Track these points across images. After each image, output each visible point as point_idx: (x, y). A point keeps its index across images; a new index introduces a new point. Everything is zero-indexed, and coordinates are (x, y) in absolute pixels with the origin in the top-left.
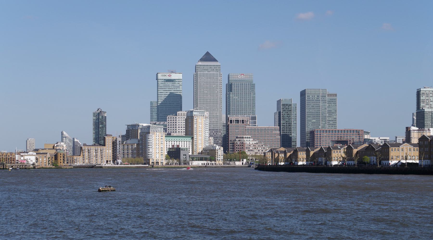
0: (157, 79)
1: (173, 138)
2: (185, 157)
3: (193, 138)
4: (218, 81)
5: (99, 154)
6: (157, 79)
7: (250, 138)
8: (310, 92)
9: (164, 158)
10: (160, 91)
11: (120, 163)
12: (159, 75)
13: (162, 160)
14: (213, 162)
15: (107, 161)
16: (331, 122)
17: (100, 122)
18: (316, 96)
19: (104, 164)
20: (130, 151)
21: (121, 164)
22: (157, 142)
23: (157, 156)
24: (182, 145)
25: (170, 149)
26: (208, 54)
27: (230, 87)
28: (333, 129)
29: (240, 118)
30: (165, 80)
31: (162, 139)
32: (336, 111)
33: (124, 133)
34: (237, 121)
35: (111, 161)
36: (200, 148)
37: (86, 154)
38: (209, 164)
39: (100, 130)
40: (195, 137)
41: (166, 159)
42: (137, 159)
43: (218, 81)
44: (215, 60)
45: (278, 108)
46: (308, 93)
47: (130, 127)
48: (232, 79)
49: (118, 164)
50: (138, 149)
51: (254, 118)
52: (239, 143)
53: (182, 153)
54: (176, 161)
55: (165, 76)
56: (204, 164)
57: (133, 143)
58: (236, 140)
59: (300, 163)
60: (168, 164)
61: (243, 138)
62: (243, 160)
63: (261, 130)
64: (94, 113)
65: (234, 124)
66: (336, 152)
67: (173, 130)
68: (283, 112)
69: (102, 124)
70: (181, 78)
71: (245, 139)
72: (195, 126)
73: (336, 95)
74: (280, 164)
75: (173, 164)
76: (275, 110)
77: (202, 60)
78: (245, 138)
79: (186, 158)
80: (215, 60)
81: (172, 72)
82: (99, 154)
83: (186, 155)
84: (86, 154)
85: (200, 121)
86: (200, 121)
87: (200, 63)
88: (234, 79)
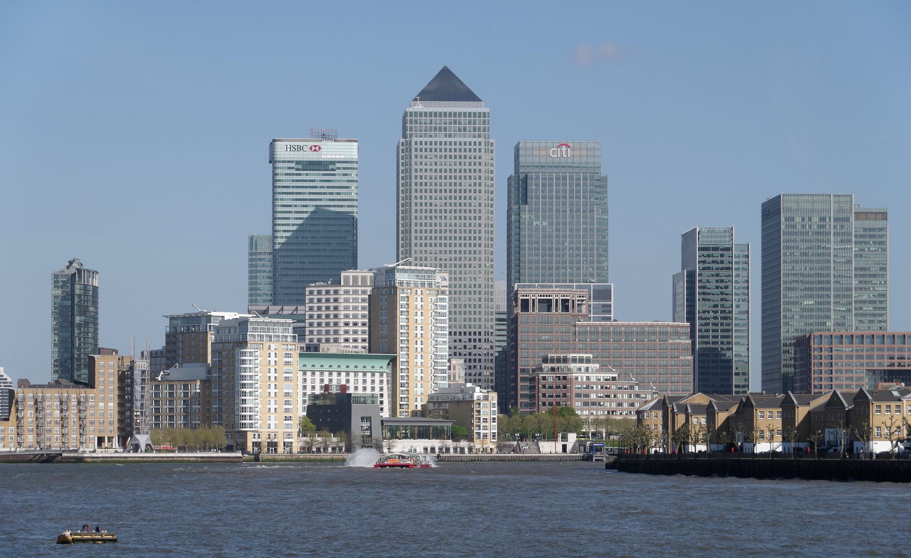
0: (272, 161)
1: (326, 363)
2: (366, 425)
3: (393, 361)
4: (483, 167)
5: (73, 414)
6: (272, 161)
7: (588, 361)
8: (794, 206)
9: (295, 430)
10: (284, 199)
11: (143, 447)
12: (280, 147)
13: (289, 435)
14: (464, 444)
15: (101, 440)
16: (869, 308)
17: (75, 307)
18: (816, 219)
19: (89, 450)
20: (180, 406)
21: (149, 448)
22: (273, 375)
23: (273, 422)
24: (357, 385)
25: (315, 397)
26: (445, 74)
27: (520, 188)
28: (875, 330)
29: (556, 293)
30: (298, 163)
31: (287, 363)
32: (884, 269)
33: (160, 344)
34: (547, 304)
35: (115, 440)
36: (418, 395)
37: (29, 414)
38: (448, 450)
39: (76, 331)
40: (401, 357)
41: (304, 432)
42: (204, 433)
43: (483, 167)
44: (469, 96)
45: (687, 258)
46: (789, 210)
47: (179, 322)
48: (529, 160)
49: (136, 448)
50: (205, 398)
51: (603, 294)
52: (550, 377)
53: (357, 412)
54: (335, 439)
55: (300, 148)
57: (189, 378)
58: (541, 369)
59: (762, 447)
60: (309, 450)
61: (565, 360)
62: (565, 438)
63: (628, 333)
64: (56, 276)
65: (535, 312)
66: (884, 408)
67: (327, 332)
68: (703, 271)
69: (84, 311)
70: (354, 156)
71: (572, 365)
72: (401, 320)
73: (884, 215)
74: (691, 449)
75: (325, 449)
76: (676, 267)
77: (426, 95)
78: (574, 360)
79: (370, 428)
80: (469, 96)
81: (324, 137)
82: (73, 414)
83: (369, 419)
84: (29, 414)
85: (419, 303)
86: (419, 303)
87: (420, 107)
88: (536, 160)
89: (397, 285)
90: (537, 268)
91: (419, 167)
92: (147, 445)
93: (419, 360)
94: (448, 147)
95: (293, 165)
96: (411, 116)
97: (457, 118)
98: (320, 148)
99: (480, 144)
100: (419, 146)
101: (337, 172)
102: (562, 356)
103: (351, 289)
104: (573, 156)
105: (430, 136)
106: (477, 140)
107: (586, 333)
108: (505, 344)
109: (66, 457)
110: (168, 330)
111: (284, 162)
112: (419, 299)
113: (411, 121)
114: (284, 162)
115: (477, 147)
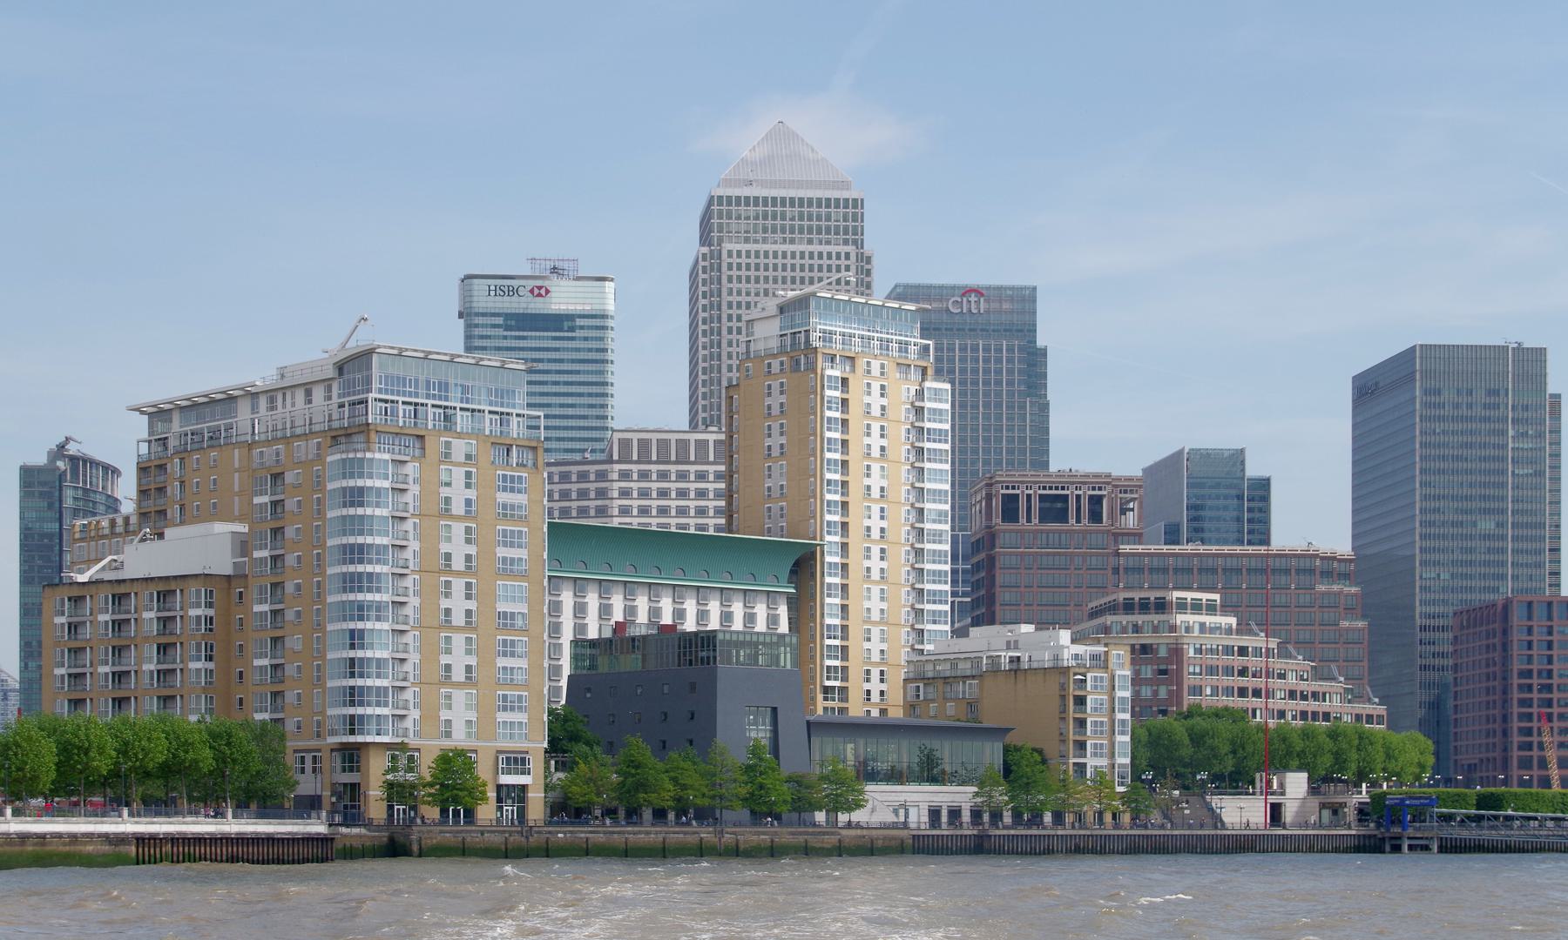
13: (517, 762)
30: (508, 316)
56: (955, 813)
65: (1031, 523)
71: (1180, 619)
89: (816, 343)
91: (735, 298)
93: (875, 564)
95: (500, 321)
96: (720, 204)
97: (805, 209)
98: (547, 292)
99: (847, 256)
101: (578, 333)
102: (1153, 595)
103: (635, 468)
104: (988, 311)
105: (756, 241)
106: (843, 249)
111: (484, 315)
112: (876, 387)
113: (720, 213)
114: (484, 315)
115: (843, 262)
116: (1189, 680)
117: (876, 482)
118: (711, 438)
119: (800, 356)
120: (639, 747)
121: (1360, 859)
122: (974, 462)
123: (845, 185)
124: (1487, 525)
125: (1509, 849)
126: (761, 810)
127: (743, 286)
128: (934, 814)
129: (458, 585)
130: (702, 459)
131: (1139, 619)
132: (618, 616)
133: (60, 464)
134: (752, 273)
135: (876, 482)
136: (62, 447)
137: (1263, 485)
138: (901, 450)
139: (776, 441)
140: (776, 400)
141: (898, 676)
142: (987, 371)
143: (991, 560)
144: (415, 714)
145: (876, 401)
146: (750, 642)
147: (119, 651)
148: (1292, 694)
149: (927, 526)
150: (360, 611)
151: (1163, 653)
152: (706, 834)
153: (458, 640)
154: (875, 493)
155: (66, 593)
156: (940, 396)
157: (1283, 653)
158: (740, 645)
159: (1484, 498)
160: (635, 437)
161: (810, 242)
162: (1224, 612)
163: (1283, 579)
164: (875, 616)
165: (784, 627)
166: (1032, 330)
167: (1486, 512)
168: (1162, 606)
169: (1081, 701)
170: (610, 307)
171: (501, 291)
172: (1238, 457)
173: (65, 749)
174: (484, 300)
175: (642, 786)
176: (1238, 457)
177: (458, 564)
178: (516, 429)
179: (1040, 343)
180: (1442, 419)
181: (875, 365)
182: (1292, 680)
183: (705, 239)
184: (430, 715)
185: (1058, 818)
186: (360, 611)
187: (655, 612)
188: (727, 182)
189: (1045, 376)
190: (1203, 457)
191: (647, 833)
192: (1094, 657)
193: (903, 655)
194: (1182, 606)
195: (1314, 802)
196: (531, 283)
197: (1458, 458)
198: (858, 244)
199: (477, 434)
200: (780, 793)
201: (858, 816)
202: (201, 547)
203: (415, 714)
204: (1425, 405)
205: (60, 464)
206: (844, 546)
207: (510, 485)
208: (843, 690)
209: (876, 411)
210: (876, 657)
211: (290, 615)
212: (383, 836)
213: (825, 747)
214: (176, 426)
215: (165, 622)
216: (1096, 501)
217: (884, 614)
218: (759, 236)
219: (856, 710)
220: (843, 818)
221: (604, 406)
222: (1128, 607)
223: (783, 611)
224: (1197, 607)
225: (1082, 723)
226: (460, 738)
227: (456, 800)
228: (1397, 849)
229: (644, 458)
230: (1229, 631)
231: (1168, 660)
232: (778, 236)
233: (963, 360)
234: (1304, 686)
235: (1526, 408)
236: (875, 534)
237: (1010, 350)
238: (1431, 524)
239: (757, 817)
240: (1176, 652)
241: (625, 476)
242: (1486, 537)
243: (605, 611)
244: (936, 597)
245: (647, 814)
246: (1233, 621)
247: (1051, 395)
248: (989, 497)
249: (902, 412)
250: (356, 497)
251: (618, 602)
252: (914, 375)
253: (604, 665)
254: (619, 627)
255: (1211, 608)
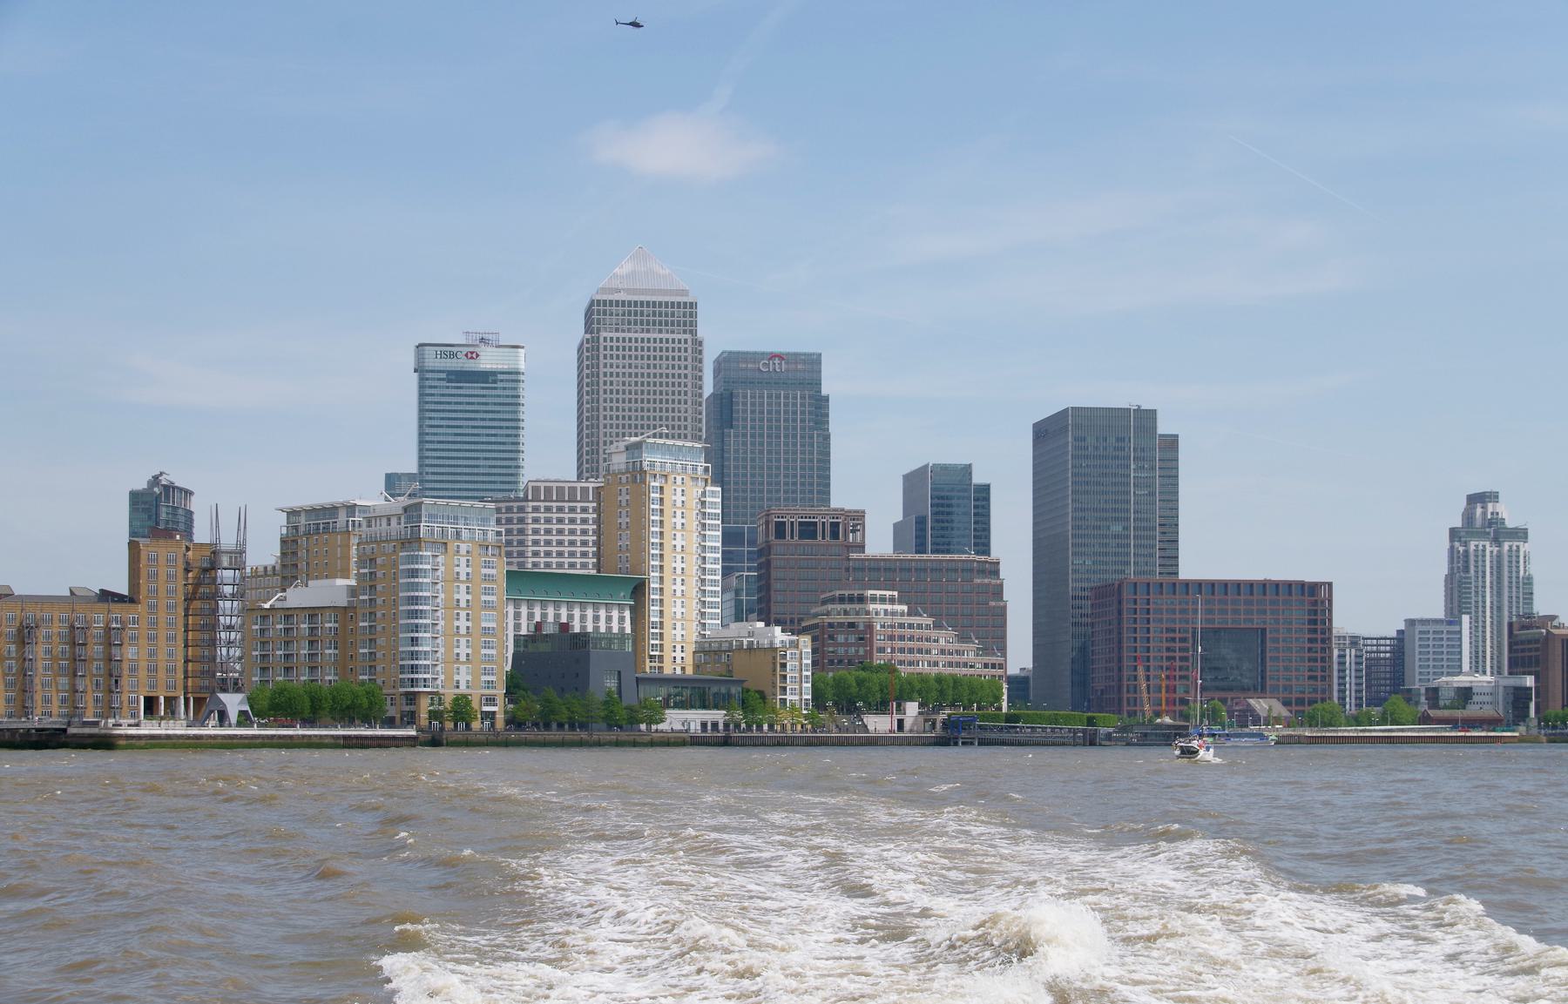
11: (233, 716)
13: (491, 700)
15: (151, 704)
18: (1112, 440)
21: (244, 719)
30: (449, 373)
47: (303, 520)
49: (223, 717)
56: (715, 725)
62: (900, 709)
71: (872, 607)
90: (761, 491)
91: (608, 370)
92: (242, 713)
93: (679, 588)
94: (646, 345)
95: (444, 376)
100: (609, 344)
101: (500, 385)
107: (863, 570)
108: (577, 630)
109: (74, 735)
110: (284, 531)
115: (683, 345)
116: (877, 644)
117: (679, 543)
118: (591, 486)
119: (637, 475)
120: (551, 693)
121: (937, 749)
122: (777, 476)
123: (684, 292)
124: (1117, 528)
125: (1003, 743)
126: (611, 723)
127: (614, 361)
128: (704, 725)
129: (463, 614)
130: (585, 499)
131: (848, 607)
132: (537, 618)
133: (156, 490)
134: (621, 353)
135: (679, 543)
136: (156, 478)
137: (984, 491)
138: (694, 525)
139: (624, 520)
140: (624, 498)
141: (691, 648)
142: (786, 412)
143: (768, 562)
144: (442, 677)
145: (679, 498)
146: (609, 638)
147: (287, 643)
148: (943, 652)
149: (708, 566)
150: (417, 628)
151: (861, 628)
152: (584, 735)
153: (463, 641)
154: (679, 549)
155: (259, 614)
156: (715, 495)
157: (937, 626)
158: (601, 639)
159: (1115, 510)
160: (542, 485)
161: (660, 331)
162: (900, 603)
163: (953, 575)
164: (679, 616)
165: (628, 630)
166: (818, 384)
167: (1116, 519)
168: (861, 599)
169: (784, 666)
170: (522, 366)
171: (444, 355)
172: (967, 470)
173: (312, 699)
174: (432, 361)
175: (552, 712)
176: (967, 470)
177: (463, 604)
178: (491, 537)
179: (824, 393)
180: (1087, 457)
181: (679, 479)
182: (942, 642)
183: (588, 329)
184: (449, 677)
185: (771, 727)
186: (417, 628)
187: (557, 616)
188: (603, 290)
189: (827, 415)
190: (945, 469)
191: (554, 735)
192: (791, 642)
193: (694, 637)
194: (874, 599)
195: (921, 719)
196: (465, 350)
197: (1098, 484)
198: (693, 333)
199: (472, 540)
200: (621, 715)
201: (661, 727)
202: (332, 591)
203: (442, 677)
204: (1075, 448)
205: (156, 490)
206: (661, 578)
207: (487, 565)
208: (661, 657)
209: (679, 504)
210: (679, 638)
211: (379, 628)
212: (429, 736)
213: (644, 691)
214: (303, 520)
215: (312, 629)
216: (835, 526)
217: (686, 609)
218: (626, 327)
219: (668, 671)
220: (654, 727)
221: (517, 436)
222: (842, 600)
223: (627, 614)
224: (883, 600)
225: (785, 677)
226: (463, 689)
227: (463, 719)
228: (956, 744)
229: (548, 498)
230: (902, 614)
231: (864, 632)
232: (639, 327)
233: (769, 404)
234: (950, 647)
235: (1143, 450)
236: (679, 571)
237: (803, 397)
238: (1079, 527)
239: (610, 727)
240: (869, 627)
241: (536, 509)
242: (1116, 537)
243: (531, 616)
244: (713, 605)
245: (554, 726)
246: (905, 608)
247: (834, 427)
248: (767, 523)
249: (693, 504)
250: (414, 573)
251: (537, 611)
252: (701, 483)
253: (531, 648)
254: (538, 626)
255: (892, 601)
